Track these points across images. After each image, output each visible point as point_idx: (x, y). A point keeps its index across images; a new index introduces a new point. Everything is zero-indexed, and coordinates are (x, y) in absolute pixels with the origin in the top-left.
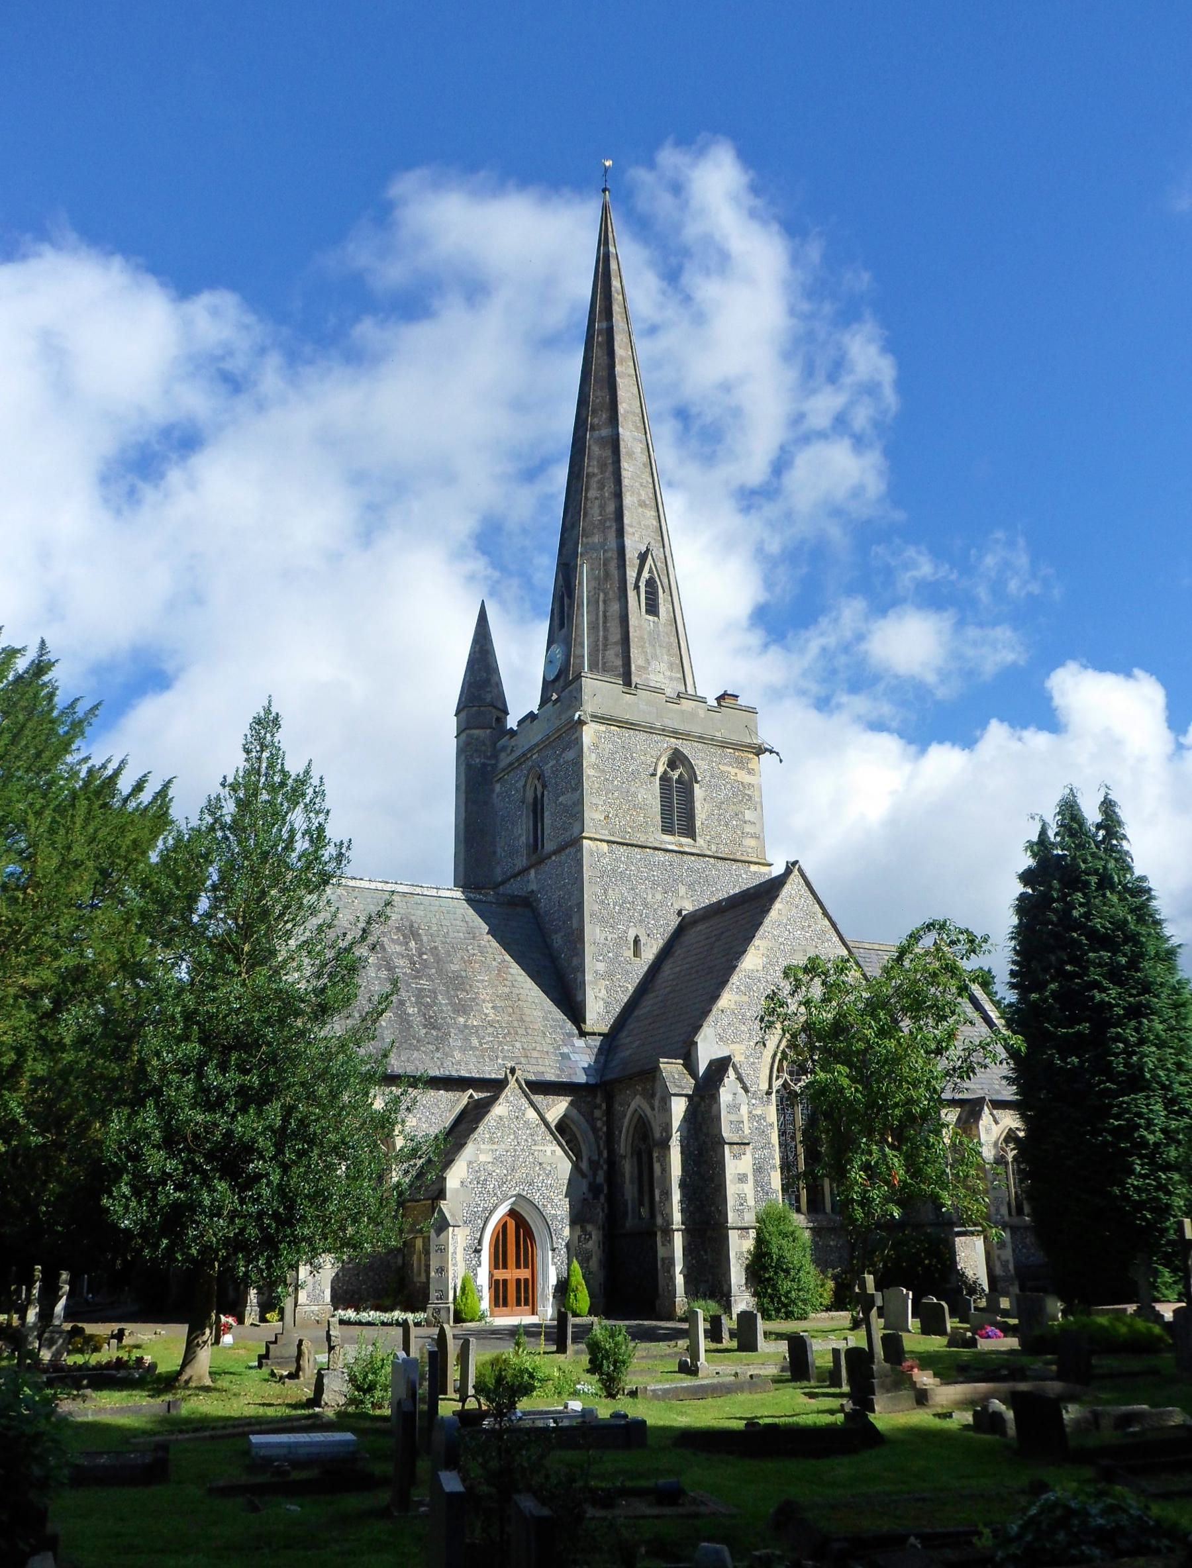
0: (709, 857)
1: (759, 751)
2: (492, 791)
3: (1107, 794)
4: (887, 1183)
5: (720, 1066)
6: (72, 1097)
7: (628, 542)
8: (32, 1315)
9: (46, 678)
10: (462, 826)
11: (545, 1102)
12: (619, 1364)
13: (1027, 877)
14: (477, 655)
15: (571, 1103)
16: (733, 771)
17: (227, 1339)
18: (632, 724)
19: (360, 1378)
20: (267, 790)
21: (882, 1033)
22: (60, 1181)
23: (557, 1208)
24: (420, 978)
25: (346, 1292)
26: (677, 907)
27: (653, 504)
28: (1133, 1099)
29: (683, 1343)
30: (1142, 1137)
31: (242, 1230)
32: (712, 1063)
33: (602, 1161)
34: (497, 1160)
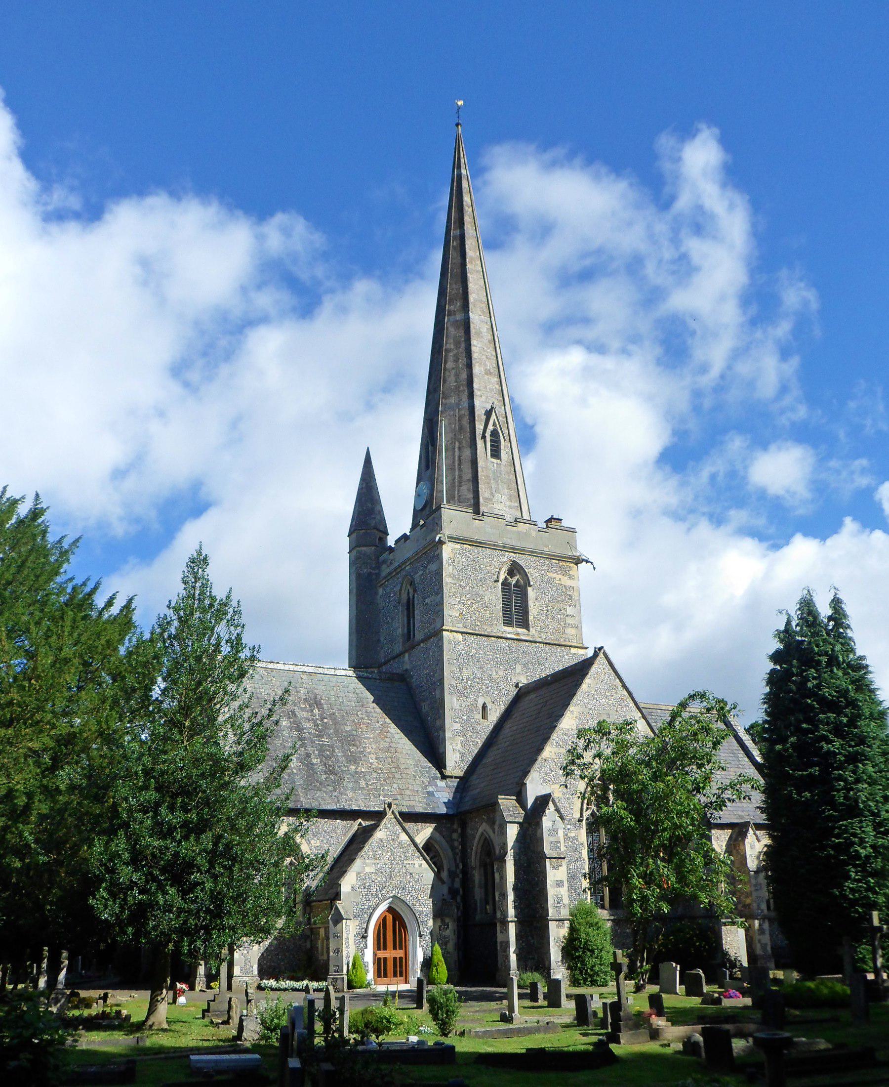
0: (540, 642)
1: (578, 561)
2: (376, 593)
3: (836, 594)
4: (660, 887)
5: (543, 801)
6: (67, 828)
7: (477, 402)
8: (42, 983)
9: (40, 521)
10: (354, 621)
11: (415, 828)
12: (450, 1013)
13: (776, 657)
14: (364, 490)
15: (435, 829)
16: (558, 577)
17: (182, 1000)
18: (480, 543)
19: (269, 1021)
20: (201, 609)
21: (655, 777)
22: (60, 887)
23: (423, 906)
24: (322, 737)
25: (270, 967)
26: (515, 681)
27: (497, 372)
28: (850, 823)
29: (505, 1002)
30: (856, 851)
31: (185, 922)
32: (537, 799)
33: (458, 871)
34: (379, 871)
